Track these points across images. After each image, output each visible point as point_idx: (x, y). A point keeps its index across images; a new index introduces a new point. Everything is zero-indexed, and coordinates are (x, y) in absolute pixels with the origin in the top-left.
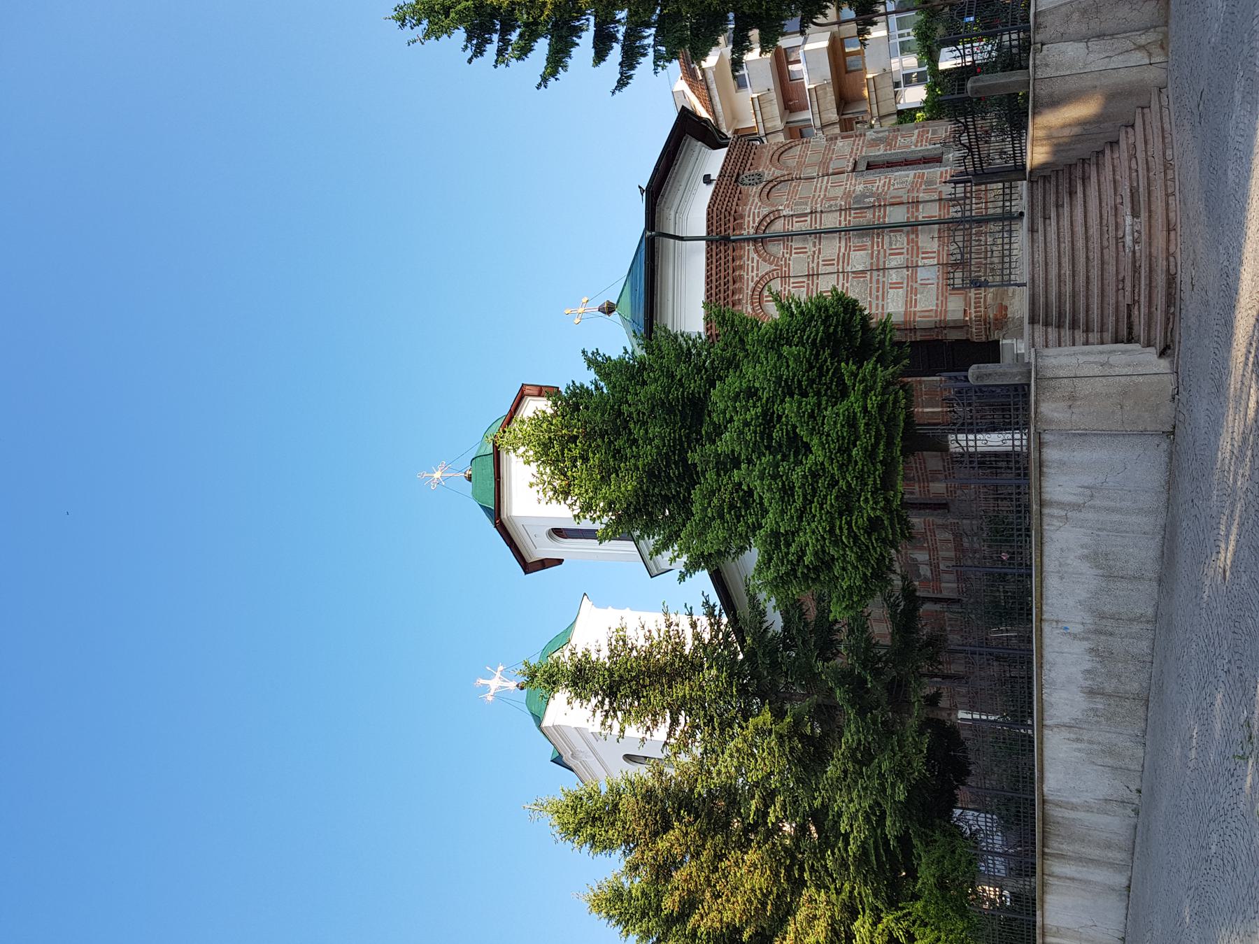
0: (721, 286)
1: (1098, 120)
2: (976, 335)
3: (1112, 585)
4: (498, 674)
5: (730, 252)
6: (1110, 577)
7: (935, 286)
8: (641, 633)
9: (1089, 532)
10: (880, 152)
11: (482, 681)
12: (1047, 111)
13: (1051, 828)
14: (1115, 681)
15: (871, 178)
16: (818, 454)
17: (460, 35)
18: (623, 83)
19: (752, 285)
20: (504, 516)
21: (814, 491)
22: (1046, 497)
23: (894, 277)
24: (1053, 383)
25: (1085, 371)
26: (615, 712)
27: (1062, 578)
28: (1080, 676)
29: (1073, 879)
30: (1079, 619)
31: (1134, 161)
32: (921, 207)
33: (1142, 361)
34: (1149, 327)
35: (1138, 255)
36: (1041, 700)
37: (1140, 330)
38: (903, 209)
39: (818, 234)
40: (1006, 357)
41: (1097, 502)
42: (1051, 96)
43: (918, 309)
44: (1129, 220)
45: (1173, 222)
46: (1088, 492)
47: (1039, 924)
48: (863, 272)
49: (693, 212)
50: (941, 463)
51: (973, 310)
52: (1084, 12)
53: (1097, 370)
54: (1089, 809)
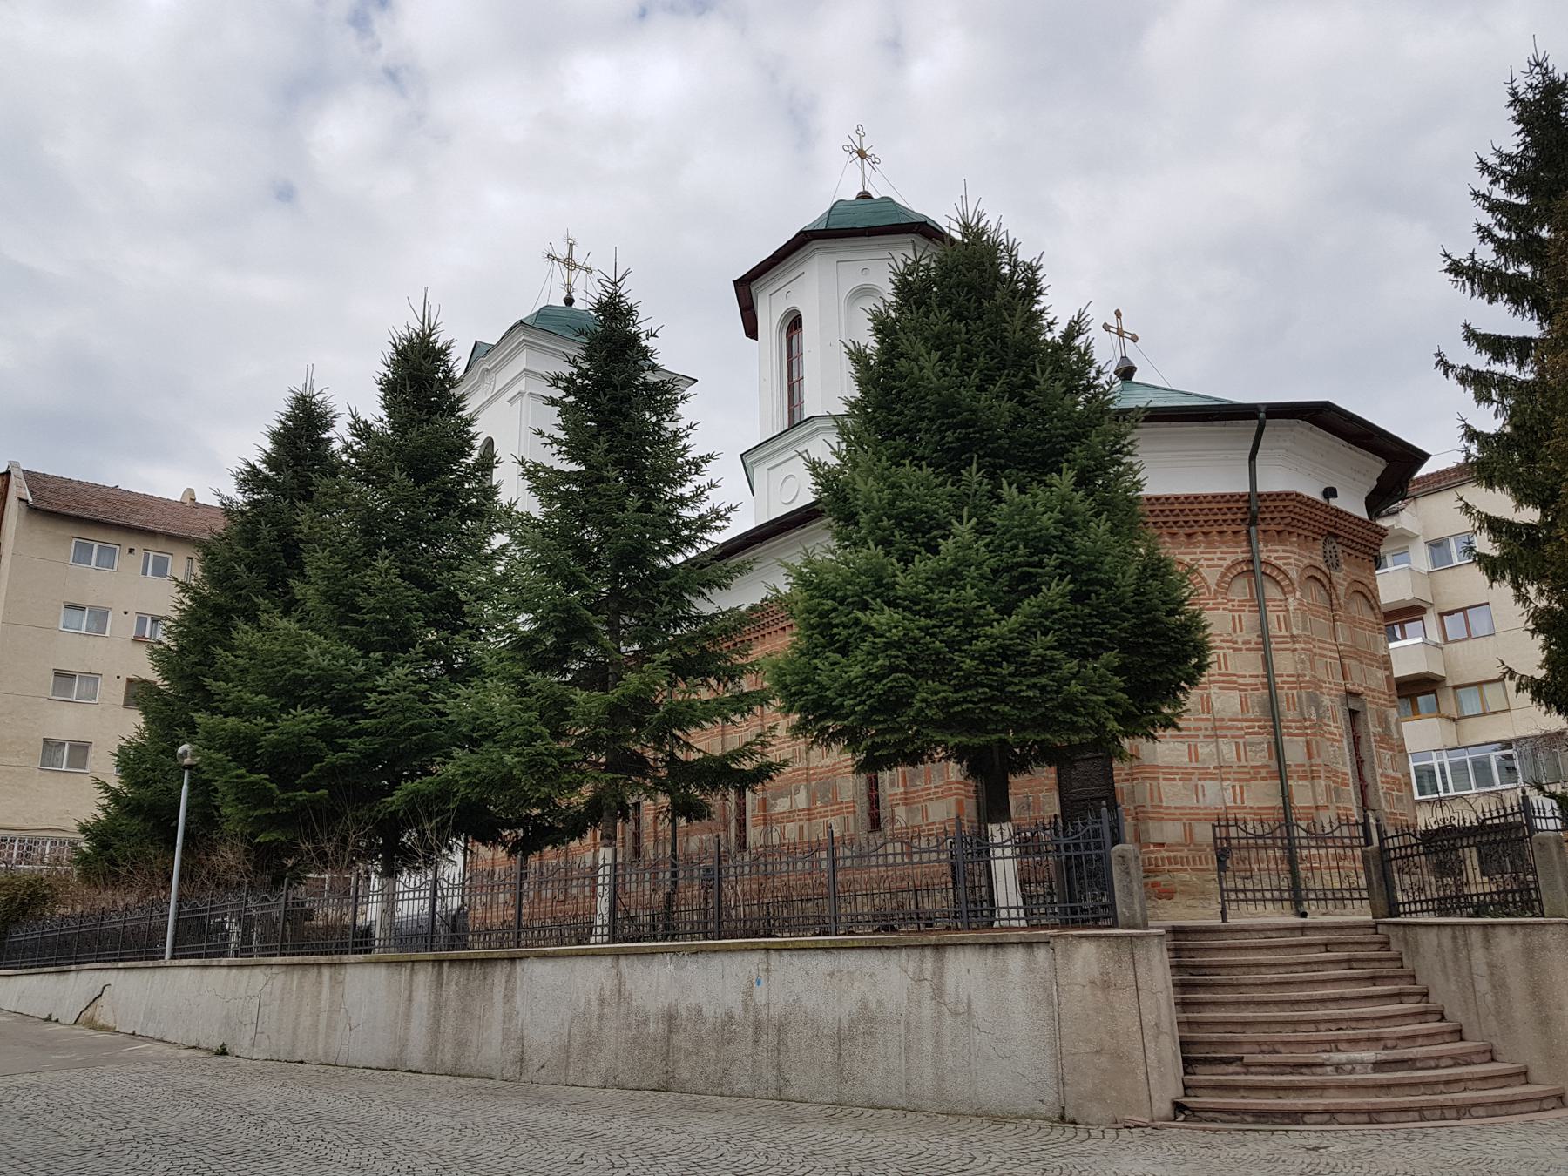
0: (1189, 515)
6: (839, 1039)
7: (1194, 803)
8: (682, 424)
9: (903, 1010)
13: (477, 971)
14: (690, 1046)
15: (1340, 715)
20: (816, 244)
22: (950, 954)
23: (1205, 750)
24: (1127, 958)
25: (1147, 1003)
27: (831, 974)
28: (692, 1001)
29: (410, 999)
33: (1168, 1084)
34: (1214, 1087)
35: (1319, 1070)
36: (653, 953)
37: (1203, 1076)
41: (948, 1020)
43: (1162, 783)
45: (1382, 1118)
47: (345, 958)
50: (937, 819)
51: (1165, 854)
53: (1149, 1019)
54: (508, 1017)
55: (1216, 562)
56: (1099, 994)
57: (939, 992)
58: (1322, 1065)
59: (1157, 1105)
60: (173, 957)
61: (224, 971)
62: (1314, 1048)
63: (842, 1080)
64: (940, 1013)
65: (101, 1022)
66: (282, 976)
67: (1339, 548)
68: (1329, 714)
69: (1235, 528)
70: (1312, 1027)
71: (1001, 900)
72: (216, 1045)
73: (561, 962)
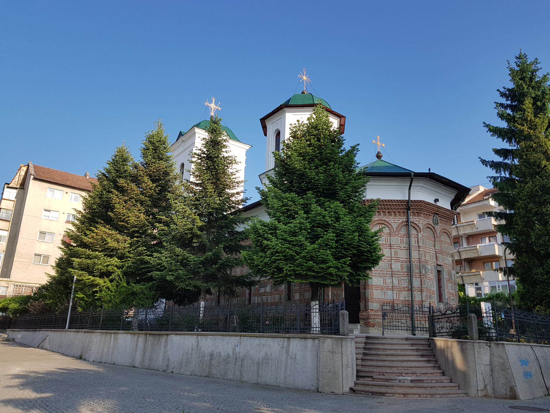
1: (454, 368)
2: (362, 314)
4: (217, 107)
5: (403, 210)
10: (445, 276)
11: (214, 100)
13: (157, 337)
15: (434, 272)
16: (310, 247)
17: (511, 86)
18: (484, 162)
19: (387, 220)
20: (286, 109)
22: (292, 340)
23: (389, 281)
24: (340, 345)
25: (345, 358)
26: (200, 159)
27: (258, 345)
29: (137, 345)
36: (208, 335)
37: (362, 381)
38: (419, 285)
39: (409, 249)
40: (352, 326)
41: (289, 360)
43: (374, 290)
44: (410, 378)
46: (294, 357)
47: (119, 331)
48: (391, 268)
49: (422, 194)
53: (345, 363)
54: (165, 353)
57: (287, 352)
58: (395, 380)
59: (344, 388)
60: (69, 328)
61: (83, 333)
62: (395, 375)
63: (258, 377)
64: (287, 358)
65: (45, 347)
66: (99, 336)
67: (439, 218)
68: (430, 271)
69: (403, 210)
70: (396, 368)
71: (313, 325)
72: (78, 354)
73: (183, 336)
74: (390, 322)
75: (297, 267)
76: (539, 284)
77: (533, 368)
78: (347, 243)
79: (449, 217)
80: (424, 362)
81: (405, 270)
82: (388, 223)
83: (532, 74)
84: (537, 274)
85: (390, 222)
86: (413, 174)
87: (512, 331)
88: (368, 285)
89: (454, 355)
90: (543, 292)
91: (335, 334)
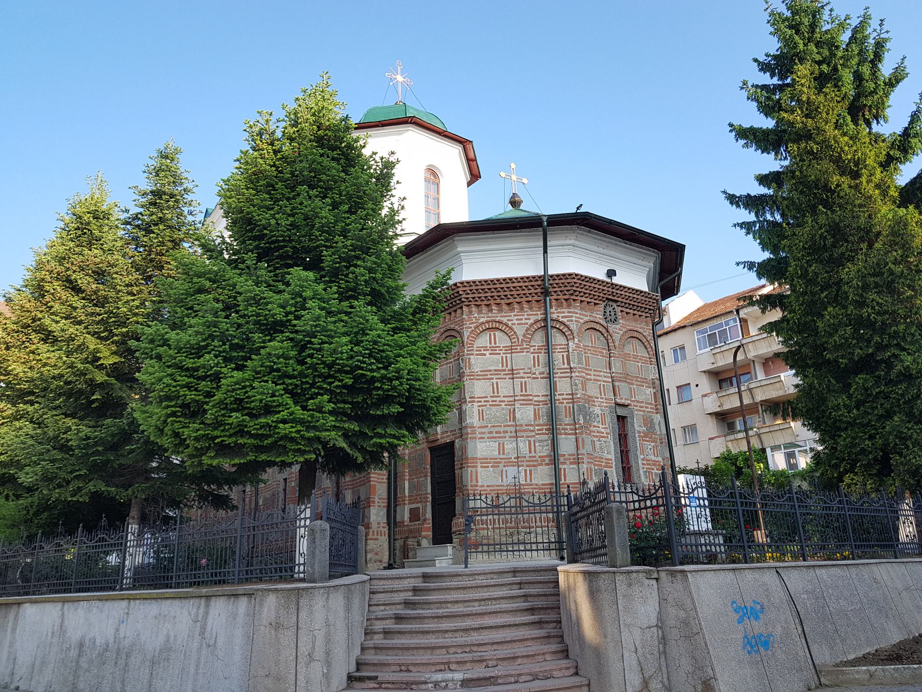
1: (580, 637)
2: (458, 523)
3: (148, 663)
5: (536, 298)
10: (637, 426)
12: (586, 587)
16: (232, 377)
18: (733, 199)
19: (505, 320)
21: (203, 378)
23: (509, 446)
24: (293, 606)
25: (304, 639)
27: (156, 617)
30: (128, 634)
31: (530, 678)
32: (575, 466)
35: (423, 686)
36: (78, 600)
38: (572, 450)
39: (550, 377)
40: (438, 549)
42: (598, 590)
43: (479, 469)
44: (459, 676)
46: (212, 642)
48: (514, 418)
49: (575, 259)
52: (685, 623)
53: (304, 649)
54: (11, 644)
55: (523, 322)
56: (273, 632)
57: (202, 633)
67: (618, 309)
69: (536, 298)
74: (512, 535)
75: (216, 429)
76: (846, 429)
77: (779, 623)
78: (324, 363)
79: (648, 307)
80: (527, 628)
81: (543, 420)
82: (507, 325)
83: (814, 16)
84: (837, 408)
85: (510, 323)
86: (545, 219)
87: (760, 536)
88: (467, 458)
89: (579, 608)
90: (855, 446)
91: (282, 579)
